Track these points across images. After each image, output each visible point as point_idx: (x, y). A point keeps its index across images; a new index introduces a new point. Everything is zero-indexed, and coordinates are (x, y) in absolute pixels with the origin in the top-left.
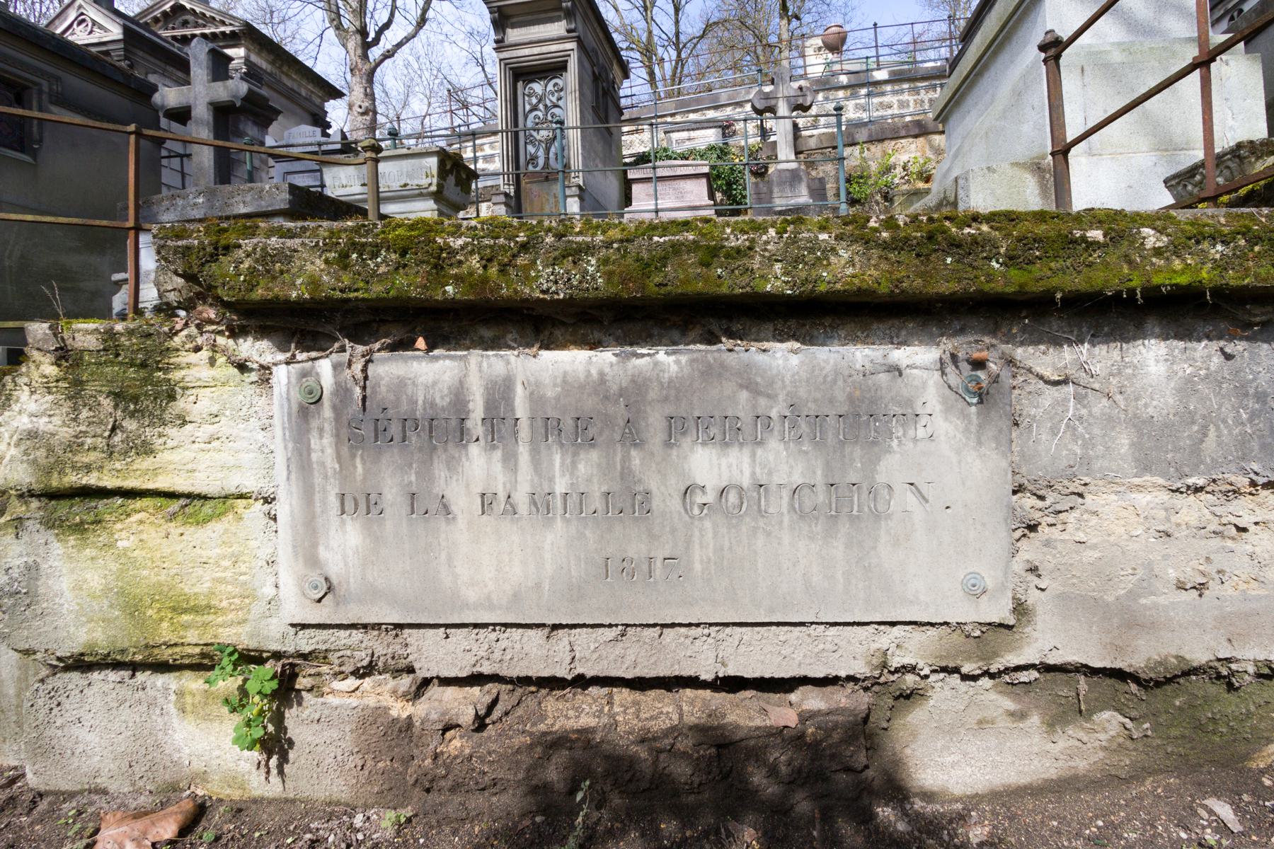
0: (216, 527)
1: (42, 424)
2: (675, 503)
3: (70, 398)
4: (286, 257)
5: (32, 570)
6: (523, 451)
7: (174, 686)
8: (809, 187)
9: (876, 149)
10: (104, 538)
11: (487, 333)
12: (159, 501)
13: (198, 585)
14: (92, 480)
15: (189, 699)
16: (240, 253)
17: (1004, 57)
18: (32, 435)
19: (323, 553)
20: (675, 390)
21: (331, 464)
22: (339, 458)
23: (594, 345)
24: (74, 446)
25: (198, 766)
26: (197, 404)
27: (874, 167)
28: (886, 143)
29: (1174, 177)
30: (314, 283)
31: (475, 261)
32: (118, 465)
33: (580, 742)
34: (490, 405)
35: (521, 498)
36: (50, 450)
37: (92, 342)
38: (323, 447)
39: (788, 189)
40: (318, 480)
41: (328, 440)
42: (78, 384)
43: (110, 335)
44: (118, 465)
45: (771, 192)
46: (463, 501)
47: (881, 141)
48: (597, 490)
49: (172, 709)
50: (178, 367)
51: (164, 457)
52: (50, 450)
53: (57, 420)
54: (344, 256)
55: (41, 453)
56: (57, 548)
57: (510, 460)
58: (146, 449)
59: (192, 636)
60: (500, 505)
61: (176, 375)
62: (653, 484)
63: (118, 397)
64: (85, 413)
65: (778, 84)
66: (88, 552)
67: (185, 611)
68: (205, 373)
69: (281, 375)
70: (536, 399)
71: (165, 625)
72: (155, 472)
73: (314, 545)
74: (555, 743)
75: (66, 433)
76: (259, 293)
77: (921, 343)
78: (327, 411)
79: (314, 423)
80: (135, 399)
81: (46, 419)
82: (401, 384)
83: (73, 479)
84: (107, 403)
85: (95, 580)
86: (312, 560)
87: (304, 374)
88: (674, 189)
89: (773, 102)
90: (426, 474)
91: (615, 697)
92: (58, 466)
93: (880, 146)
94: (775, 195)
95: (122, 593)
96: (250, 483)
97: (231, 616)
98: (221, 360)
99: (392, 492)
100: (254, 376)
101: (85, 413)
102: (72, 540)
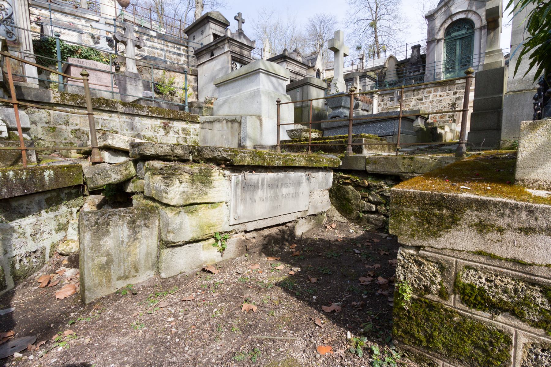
0: (217, 209)
1: (186, 189)
2: (281, 197)
3: (192, 183)
4: (244, 157)
5: (181, 223)
6: (265, 190)
7: (202, 244)
8: (143, 83)
9: (167, 73)
10: (197, 214)
11: (260, 170)
12: (205, 205)
13: (213, 221)
14: (195, 201)
15: (205, 246)
16: (238, 156)
17: (244, 81)
18: (184, 192)
19: (238, 211)
20: (282, 179)
21: (240, 194)
22: (241, 192)
23: (273, 172)
24: (192, 194)
25: (204, 260)
26: (215, 183)
27: (167, 81)
28: (171, 73)
29: (289, 130)
30: (248, 162)
31: (268, 160)
32: (201, 198)
33: (269, 236)
34: (262, 183)
35: (264, 198)
36: (187, 195)
37: (197, 171)
38: (239, 191)
39: (133, 82)
40: (238, 197)
41: (240, 190)
42: (193, 180)
43: (201, 169)
44: (201, 198)
45: (126, 81)
46: (257, 199)
47: (169, 71)
48: (273, 196)
49: (201, 249)
50: (213, 176)
51: (209, 195)
52: (187, 195)
53: (189, 189)
54: (253, 157)
55: (185, 196)
56: (187, 217)
57: (263, 191)
58: (206, 194)
59: (212, 232)
60: (262, 200)
61: (212, 178)
62: (279, 195)
63: (201, 183)
64: (195, 187)
65: (128, 32)
66: (193, 217)
67: (211, 227)
68: (218, 177)
69: (234, 178)
70: (267, 181)
71: (207, 230)
72: (207, 198)
73: (236, 210)
74: (265, 237)
75: (191, 191)
76: (241, 164)
77: (298, 172)
78: (240, 185)
79: (238, 187)
80: (204, 183)
81: (186, 189)
82: (251, 179)
83: (191, 201)
84: (199, 184)
85: (194, 223)
86: (236, 213)
87: (237, 178)
88: (96, 75)
89: (125, 40)
90: (253, 195)
91: (119, 288)
92: (188, 199)
93: (169, 73)
94: (127, 83)
95: (199, 225)
96: (224, 199)
97: (219, 226)
98: (221, 175)
99: (248, 199)
100: (226, 178)
101: (195, 187)
102: (190, 215)
